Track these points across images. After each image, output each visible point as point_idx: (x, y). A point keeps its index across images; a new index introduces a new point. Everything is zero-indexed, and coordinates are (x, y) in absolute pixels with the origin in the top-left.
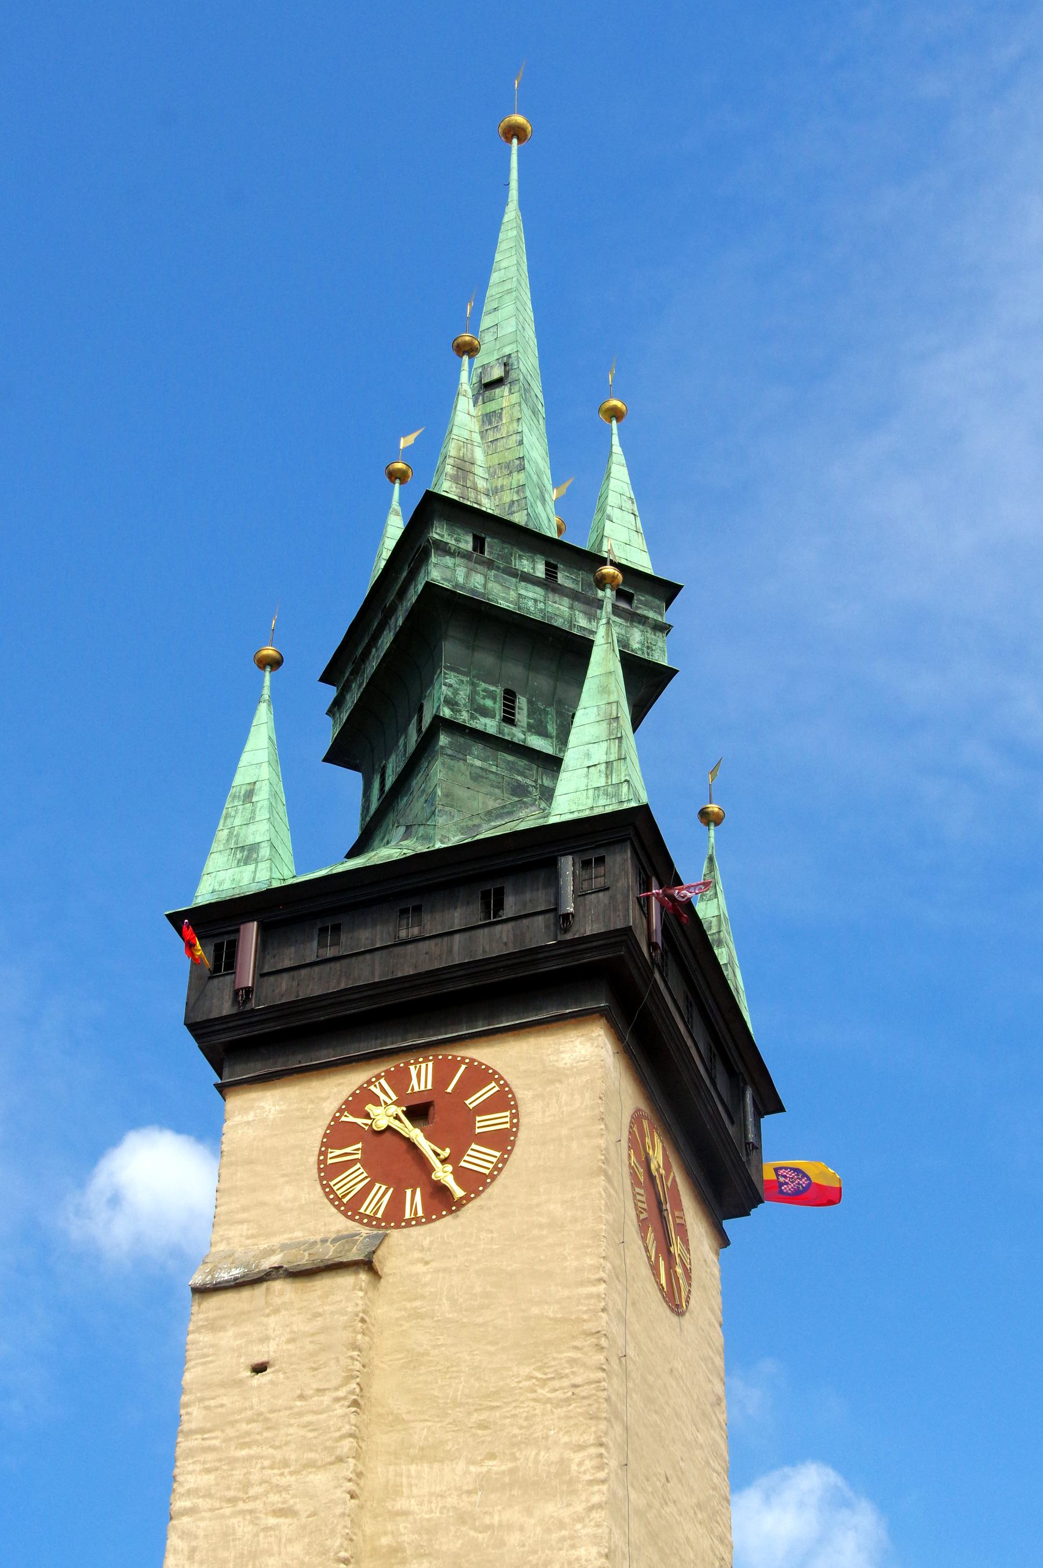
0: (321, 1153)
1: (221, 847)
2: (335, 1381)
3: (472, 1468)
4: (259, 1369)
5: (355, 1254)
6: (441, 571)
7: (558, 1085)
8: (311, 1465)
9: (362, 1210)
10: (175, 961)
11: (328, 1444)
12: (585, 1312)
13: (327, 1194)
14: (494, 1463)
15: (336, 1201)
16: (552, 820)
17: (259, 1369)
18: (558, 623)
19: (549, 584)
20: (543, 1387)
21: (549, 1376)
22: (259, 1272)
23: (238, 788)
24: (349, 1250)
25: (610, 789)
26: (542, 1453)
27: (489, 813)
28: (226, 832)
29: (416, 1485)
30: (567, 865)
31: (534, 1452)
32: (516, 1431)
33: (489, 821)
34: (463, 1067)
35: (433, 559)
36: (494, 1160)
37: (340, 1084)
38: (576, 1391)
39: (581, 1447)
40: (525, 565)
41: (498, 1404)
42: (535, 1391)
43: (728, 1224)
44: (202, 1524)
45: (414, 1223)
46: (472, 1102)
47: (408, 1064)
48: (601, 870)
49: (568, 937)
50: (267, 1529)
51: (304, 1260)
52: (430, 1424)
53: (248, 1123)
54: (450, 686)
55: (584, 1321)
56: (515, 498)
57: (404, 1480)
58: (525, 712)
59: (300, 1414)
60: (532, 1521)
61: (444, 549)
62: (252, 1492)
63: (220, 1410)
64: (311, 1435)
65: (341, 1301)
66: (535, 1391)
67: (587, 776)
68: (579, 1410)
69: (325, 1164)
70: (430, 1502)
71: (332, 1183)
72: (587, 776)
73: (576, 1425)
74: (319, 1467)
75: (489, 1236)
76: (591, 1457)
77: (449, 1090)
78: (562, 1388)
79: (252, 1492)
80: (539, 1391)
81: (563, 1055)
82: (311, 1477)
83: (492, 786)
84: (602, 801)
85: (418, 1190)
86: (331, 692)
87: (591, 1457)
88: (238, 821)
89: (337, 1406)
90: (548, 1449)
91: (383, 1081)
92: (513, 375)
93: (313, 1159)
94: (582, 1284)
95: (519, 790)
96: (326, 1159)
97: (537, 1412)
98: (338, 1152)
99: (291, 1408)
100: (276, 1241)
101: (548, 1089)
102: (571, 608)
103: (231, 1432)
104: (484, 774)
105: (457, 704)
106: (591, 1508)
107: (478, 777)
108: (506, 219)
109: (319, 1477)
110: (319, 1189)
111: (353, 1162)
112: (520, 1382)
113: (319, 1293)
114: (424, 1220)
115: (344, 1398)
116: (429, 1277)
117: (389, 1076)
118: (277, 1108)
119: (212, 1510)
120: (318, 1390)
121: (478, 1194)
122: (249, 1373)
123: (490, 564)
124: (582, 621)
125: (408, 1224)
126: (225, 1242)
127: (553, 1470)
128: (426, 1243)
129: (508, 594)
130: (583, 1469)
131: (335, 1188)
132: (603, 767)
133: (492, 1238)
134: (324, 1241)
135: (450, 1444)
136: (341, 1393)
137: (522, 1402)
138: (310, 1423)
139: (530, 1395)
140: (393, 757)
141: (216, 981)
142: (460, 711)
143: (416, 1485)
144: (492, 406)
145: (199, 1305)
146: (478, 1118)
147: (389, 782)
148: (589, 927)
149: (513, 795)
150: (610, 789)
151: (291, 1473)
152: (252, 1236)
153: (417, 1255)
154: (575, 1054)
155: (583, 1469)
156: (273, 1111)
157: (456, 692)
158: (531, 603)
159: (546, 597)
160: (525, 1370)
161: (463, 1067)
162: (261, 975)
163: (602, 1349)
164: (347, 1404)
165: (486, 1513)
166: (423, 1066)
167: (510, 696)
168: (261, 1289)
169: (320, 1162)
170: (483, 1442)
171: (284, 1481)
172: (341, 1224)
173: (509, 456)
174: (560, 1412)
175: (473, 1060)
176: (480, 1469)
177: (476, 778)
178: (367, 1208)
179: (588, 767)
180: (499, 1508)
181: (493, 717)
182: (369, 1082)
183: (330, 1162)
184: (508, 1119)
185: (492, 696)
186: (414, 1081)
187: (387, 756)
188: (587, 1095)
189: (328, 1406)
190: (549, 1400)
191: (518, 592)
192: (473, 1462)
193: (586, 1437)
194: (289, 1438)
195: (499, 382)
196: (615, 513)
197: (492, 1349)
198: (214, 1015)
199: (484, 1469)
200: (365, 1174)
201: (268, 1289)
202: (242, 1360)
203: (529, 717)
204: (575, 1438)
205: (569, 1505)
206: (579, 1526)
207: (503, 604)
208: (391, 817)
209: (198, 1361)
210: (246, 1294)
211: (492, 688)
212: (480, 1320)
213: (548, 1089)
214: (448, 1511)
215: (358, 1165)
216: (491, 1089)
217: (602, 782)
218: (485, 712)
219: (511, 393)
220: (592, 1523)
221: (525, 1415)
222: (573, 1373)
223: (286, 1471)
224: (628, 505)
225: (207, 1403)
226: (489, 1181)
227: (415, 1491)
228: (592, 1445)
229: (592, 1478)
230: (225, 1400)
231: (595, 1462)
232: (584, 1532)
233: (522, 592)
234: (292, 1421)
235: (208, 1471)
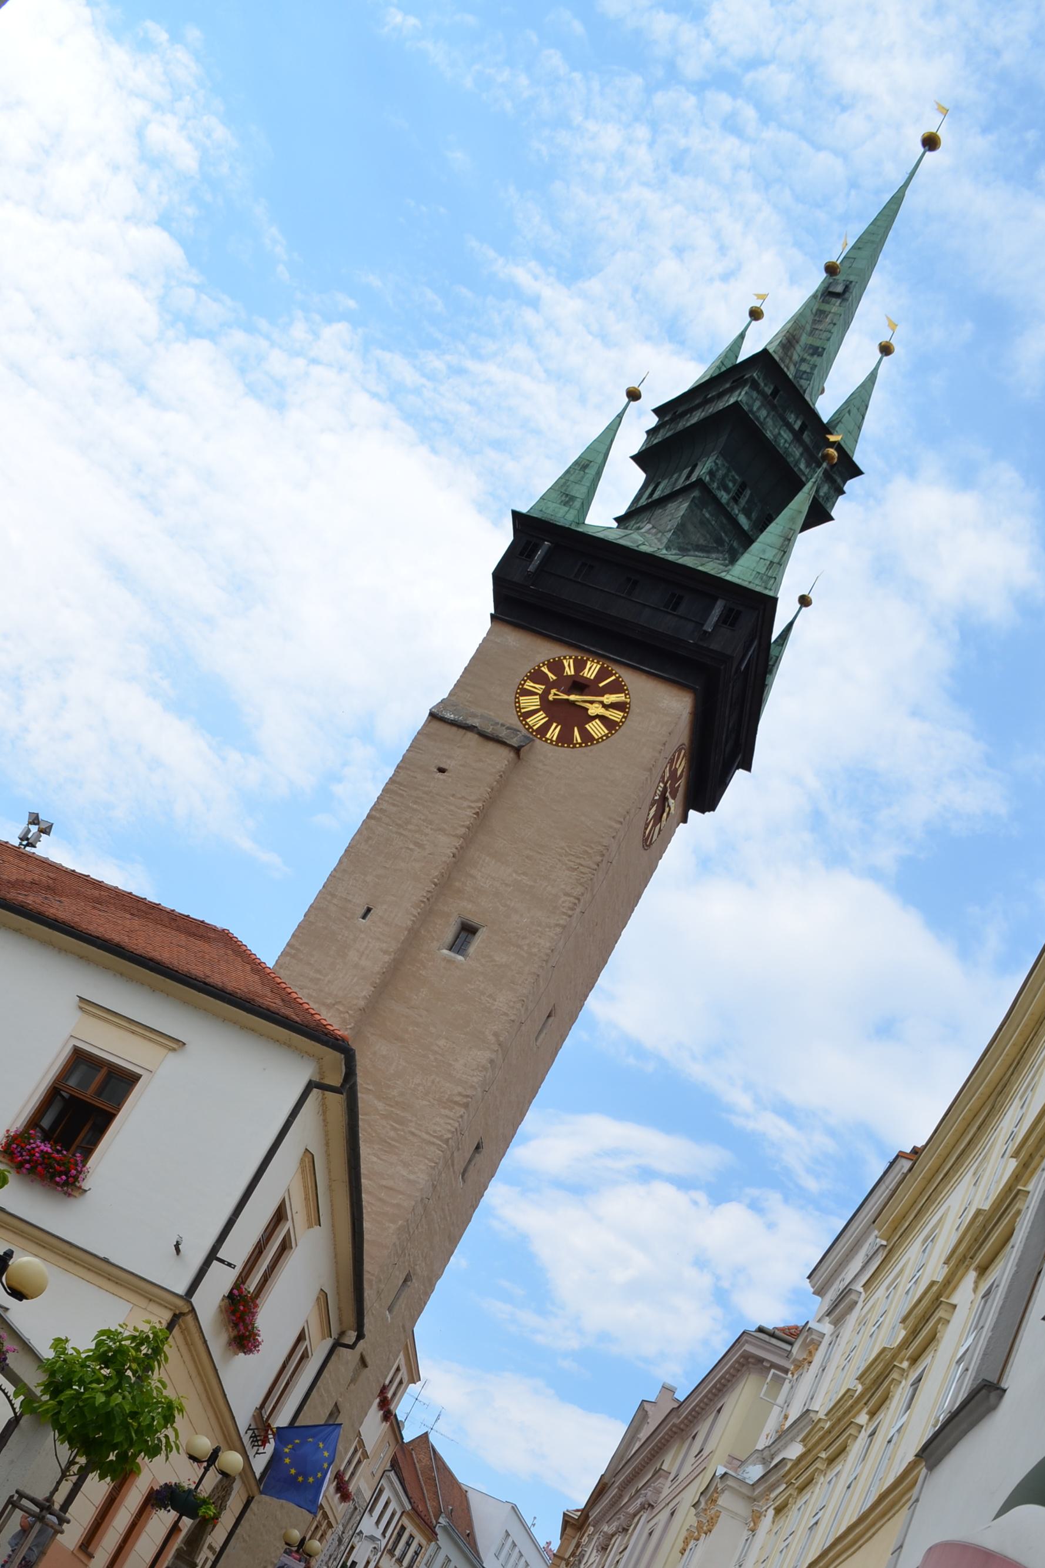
4: (442, 770)
5: (514, 742)
6: (747, 1348)
16: (728, 578)
17: (442, 770)
18: (790, 460)
19: (797, 436)
33: (696, 550)
34: (613, 678)
39: (567, 894)
40: (791, 418)
43: (692, 813)
44: (380, 829)
47: (588, 659)
49: (701, 643)
50: (408, 848)
51: (489, 730)
62: (409, 827)
77: (601, 685)
79: (409, 827)
84: (757, 582)
92: (847, 295)
94: (610, 818)
95: (719, 541)
98: (532, 684)
100: (480, 711)
102: (802, 455)
106: (557, 925)
107: (704, 523)
111: (536, 694)
117: (576, 661)
119: (387, 824)
123: (774, 407)
124: (802, 466)
134: (503, 725)
136: (473, 805)
140: (666, 481)
144: (826, 307)
147: (656, 496)
148: (714, 646)
157: (718, 469)
159: (792, 441)
161: (613, 678)
163: (603, 855)
167: (743, 487)
168: (461, 732)
171: (427, 831)
172: (514, 721)
173: (818, 343)
174: (567, 873)
185: (734, 481)
186: (586, 670)
187: (663, 479)
192: (516, 872)
195: (837, 295)
203: (747, 503)
207: (769, 435)
208: (648, 514)
217: (763, 571)
218: (727, 489)
219: (840, 305)
231: (571, 905)
233: (782, 432)
235: (394, 805)
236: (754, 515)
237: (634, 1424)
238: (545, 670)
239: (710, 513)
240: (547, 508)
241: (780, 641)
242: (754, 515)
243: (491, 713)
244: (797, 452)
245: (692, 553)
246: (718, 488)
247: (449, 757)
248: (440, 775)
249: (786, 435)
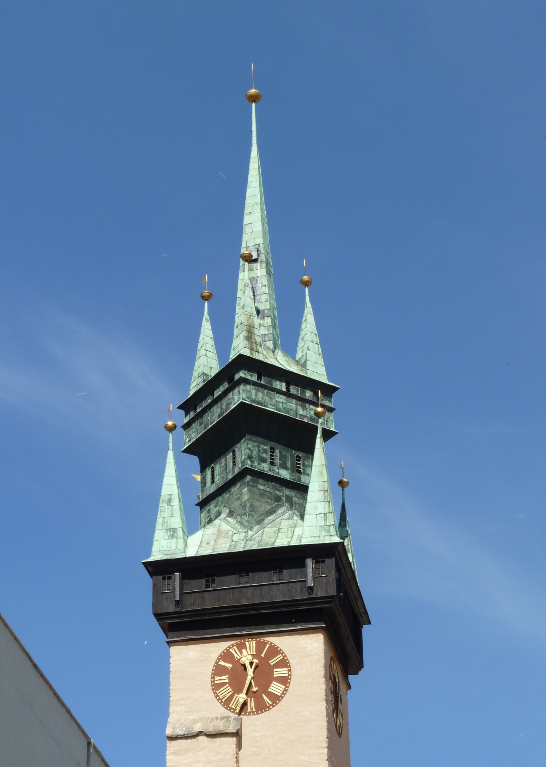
0: (212, 678)
1: (160, 528)
9: (230, 706)
10: (147, 581)
13: (216, 697)
19: (288, 394)
24: (229, 727)
25: (326, 528)
27: (267, 512)
28: (161, 519)
30: (309, 562)
33: (267, 516)
34: (268, 645)
36: (282, 690)
37: (217, 646)
43: (351, 678)
46: (272, 662)
49: (311, 596)
56: (267, 333)
67: (316, 519)
71: (217, 692)
72: (316, 519)
77: (263, 656)
83: (268, 498)
84: (324, 533)
85: (253, 699)
88: (166, 515)
91: (235, 647)
95: (278, 499)
98: (219, 678)
100: (195, 716)
102: (296, 405)
104: (264, 493)
105: (252, 458)
107: (262, 494)
110: (212, 693)
121: (277, 704)
124: (301, 412)
129: (272, 401)
131: (219, 694)
142: (254, 461)
145: (170, 743)
149: (276, 502)
150: (326, 528)
157: (252, 453)
158: (281, 405)
161: (268, 645)
162: (182, 594)
166: (251, 642)
169: (212, 682)
172: (222, 711)
175: (271, 643)
177: (261, 495)
178: (232, 705)
181: (266, 462)
182: (229, 647)
183: (216, 682)
185: (265, 451)
191: (277, 403)
200: (231, 690)
210: (189, 741)
211: (266, 447)
215: (228, 685)
216: (279, 657)
217: (322, 524)
218: (264, 461)
233: (277, 399)
236: (289, 465)
237: (359, 602)
238: (222, 663)
239: (262, 485)
240: (163, 547)
241: (343, 523)
242: (289, 465)
244: (293, 404)
245: (266, 521)
246: (259, 464)
249: (281, 399)
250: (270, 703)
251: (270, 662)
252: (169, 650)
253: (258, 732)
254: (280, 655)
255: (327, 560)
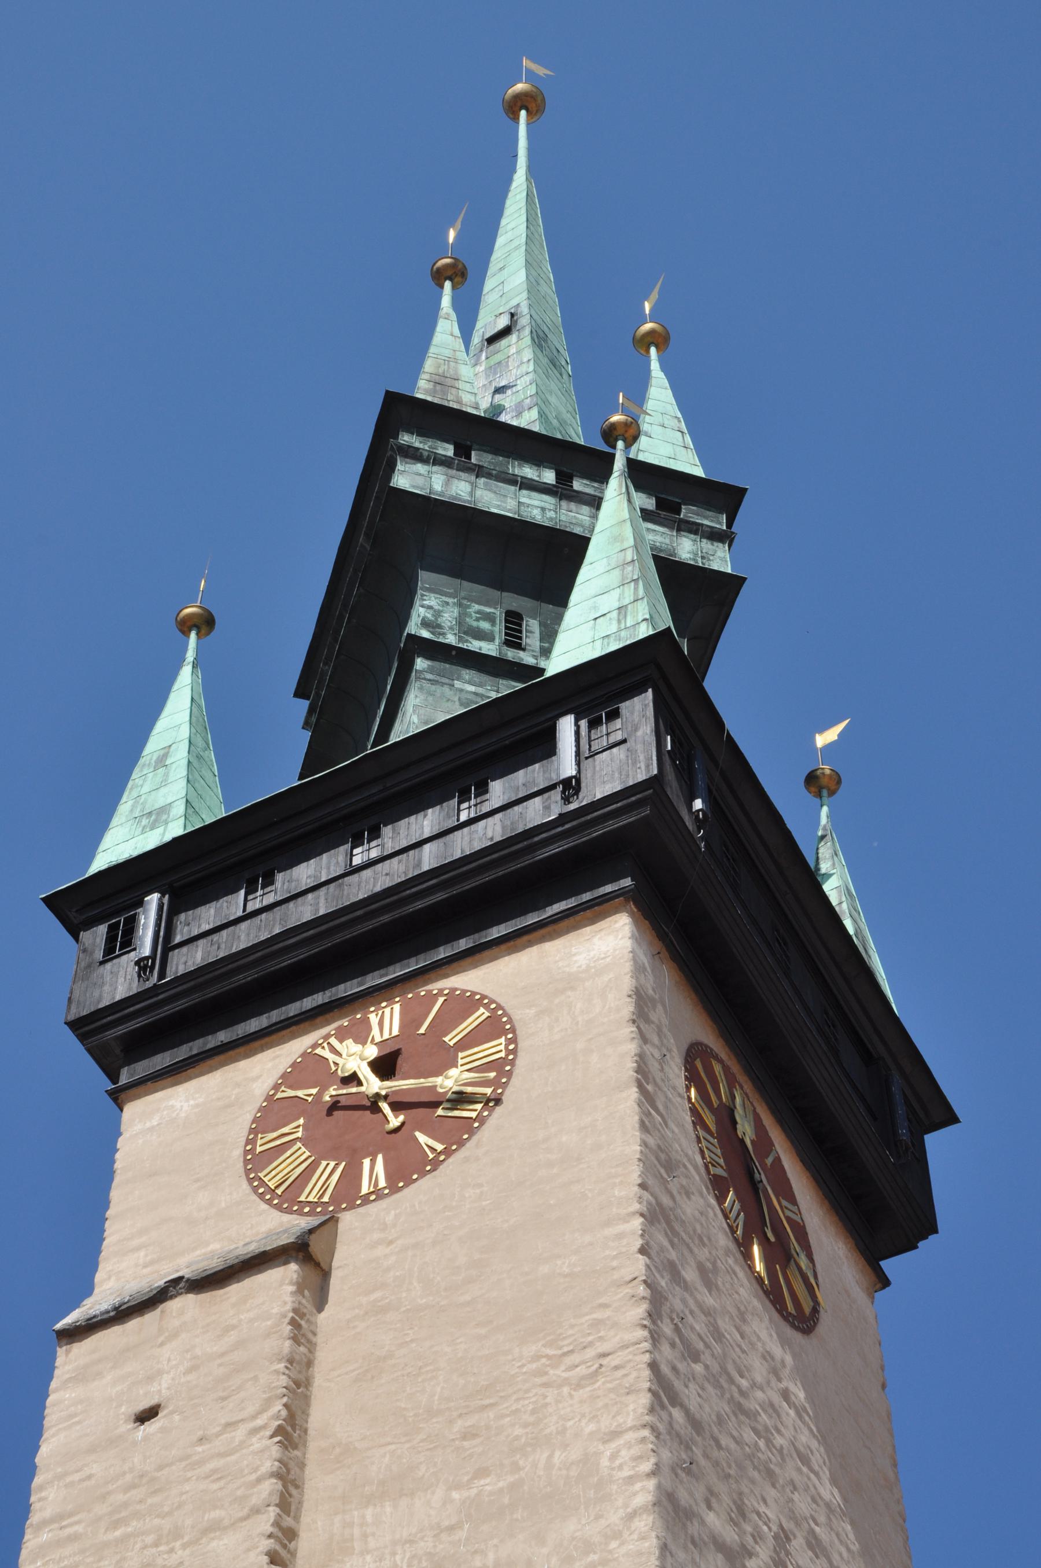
2: (251, 1409)
3: (455, 1495)
4: (146, 1416)
7: (569, 993)
8: (214, 1528)
11: (239, 1493)
12: (615, 1257)
13: (255, 1189)
14: (488, 1480)
15: (257, 1185)
17: (146, 1416)
20: (554, 1366)
21: (565, 1349)
22: (151, 1291)
23: (149, 757)
26: (557, 1454)
28: (130, 803)
29: (373, 1534)
30: (566, 726)
31: (545, 1455)
32: (518, 1431)
35: (400, 466)
38: (605, 1361)
41: (491, 1401)
42: (546, 1373)
43: (884, 1264)
45: (373, 1197)
48: (618, 723)
52: (393, 1447)
53: (152, 1129)
54: (430, 607)
55: (614, 1269)
57: (357, 1531)
58: (537, 634)
59: (201, 1463)
60: (545, 1551)
61: (413, 455)
63: (87, 1483)
64: (215, 1486)
65: (263, 1304)
66: (546, 1373)
68: (609, 1385)
69: (254, 1154)
70: (394, 1554)
73: (606, 1406)
74: (225, 1528)
75: (478, 1191)
76: (629, 1445)
77: (422, 1031)
78: (584, 1362)
80: (551, 1372)
81: (575, 958)
82: (214, 1544)
85: (380, 1158)
86: (305, 704)
87: (629, 1445)
88: (146, 789)
89: (254, 1440)
90: (565, 1446)
93: (238, 1152)
96: (254, 1148)
97: (548, 1400)
99: (189, 1457)
101: (557, 1001)
103: (101, 1509)
105: (439, 626)
106: (632, 1516)
108: (514, 185)
109: (226, 1541)
112: (523, 1366)
113: (233, 1300)
114: (387, 1191)
115: (264, 1427)
116: (393, 1258)
118: (192, 1102)
120: (228, 1425)
121: (461, 1143)
122: (131, 1425)
125: (366, 1200)
126: (113, 1279)
127: (574, 1472)
128: (390, 1218)
129: (505, 502)
130: (617, 1463)
131: (266, 1179)
132: (615, 614)
133: (482, 1192)
135: (423, 1468)
136: (259, 1422)
137: (527, 1391)
138: (214, 1471)
139: (538, 1380)
141: (108, 966)
143: (373, 1534)
145: (68, 1352)
146: (460, 1055)
151: (184, 1547)
152: (152, 1263)
153: (376, 1236)
154: (592, 954)
155: (617, 1463)
156: (185, 1108)
157: (438, 614)
160: (532, 1349)
161: (441, 1000)
164: (268, 1433)
165: (476, 1552)
168: (150, 1318)
170: (471, 1456)
174: (584, 1393)
176: (465, 1494)
179: (596, 619)
180: (495, 1541)
182: (315, 1046)
183: (259, 1149)
184: (502, 1047)
185: (490, 618)
188: (610, 996)
189: (242, 1442)
190: (566, 1381)
192: (458, 1486)
193: (620, 1419)
194: (184, 1497)
196: (656, 430)
197: (483, 1331)
198: (105, 1002)
199: (474, 1492)
200: (308, 1154)
201: (162, 1312)
202: (123, 1409)
203: (541, 640)
204: (606, 1423)
205: (598, 1517)
206: (614, 1545)
209: (61, 1426)
211: (488, 610)
212: (467, 1297)
213: (557, 1001)
214: (420, 1561)
215: (299, 1144)
220: (635, 1536)
221: (531, 1407)
222: (601, 1338)
223: (178, 1544)
224: (674, 423)
225: (68, 1479)
226: (476, 1125)
227: (372, 1543)
228: (631, 1428)
229: (632, 1473)
230: (95, 1469)
232: (623, 1550)
234: (189, 1474)
243: (211, 1247)
247: (150, 1379)
248: (152, 1427)
250: (440, 1147)
251: (446, 1039)
252: (121, 1117)
253: (391, 1242)
254: (482, 1010)
255: (625, 707)
